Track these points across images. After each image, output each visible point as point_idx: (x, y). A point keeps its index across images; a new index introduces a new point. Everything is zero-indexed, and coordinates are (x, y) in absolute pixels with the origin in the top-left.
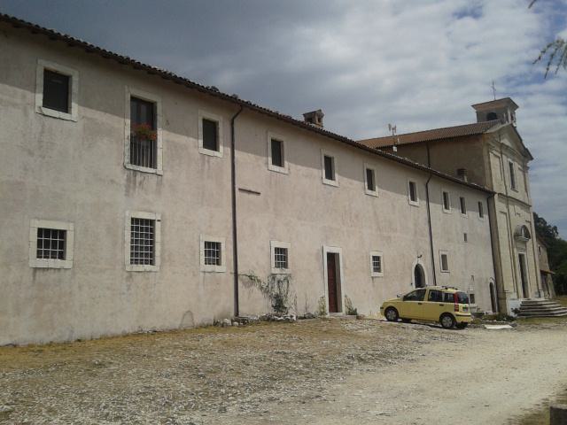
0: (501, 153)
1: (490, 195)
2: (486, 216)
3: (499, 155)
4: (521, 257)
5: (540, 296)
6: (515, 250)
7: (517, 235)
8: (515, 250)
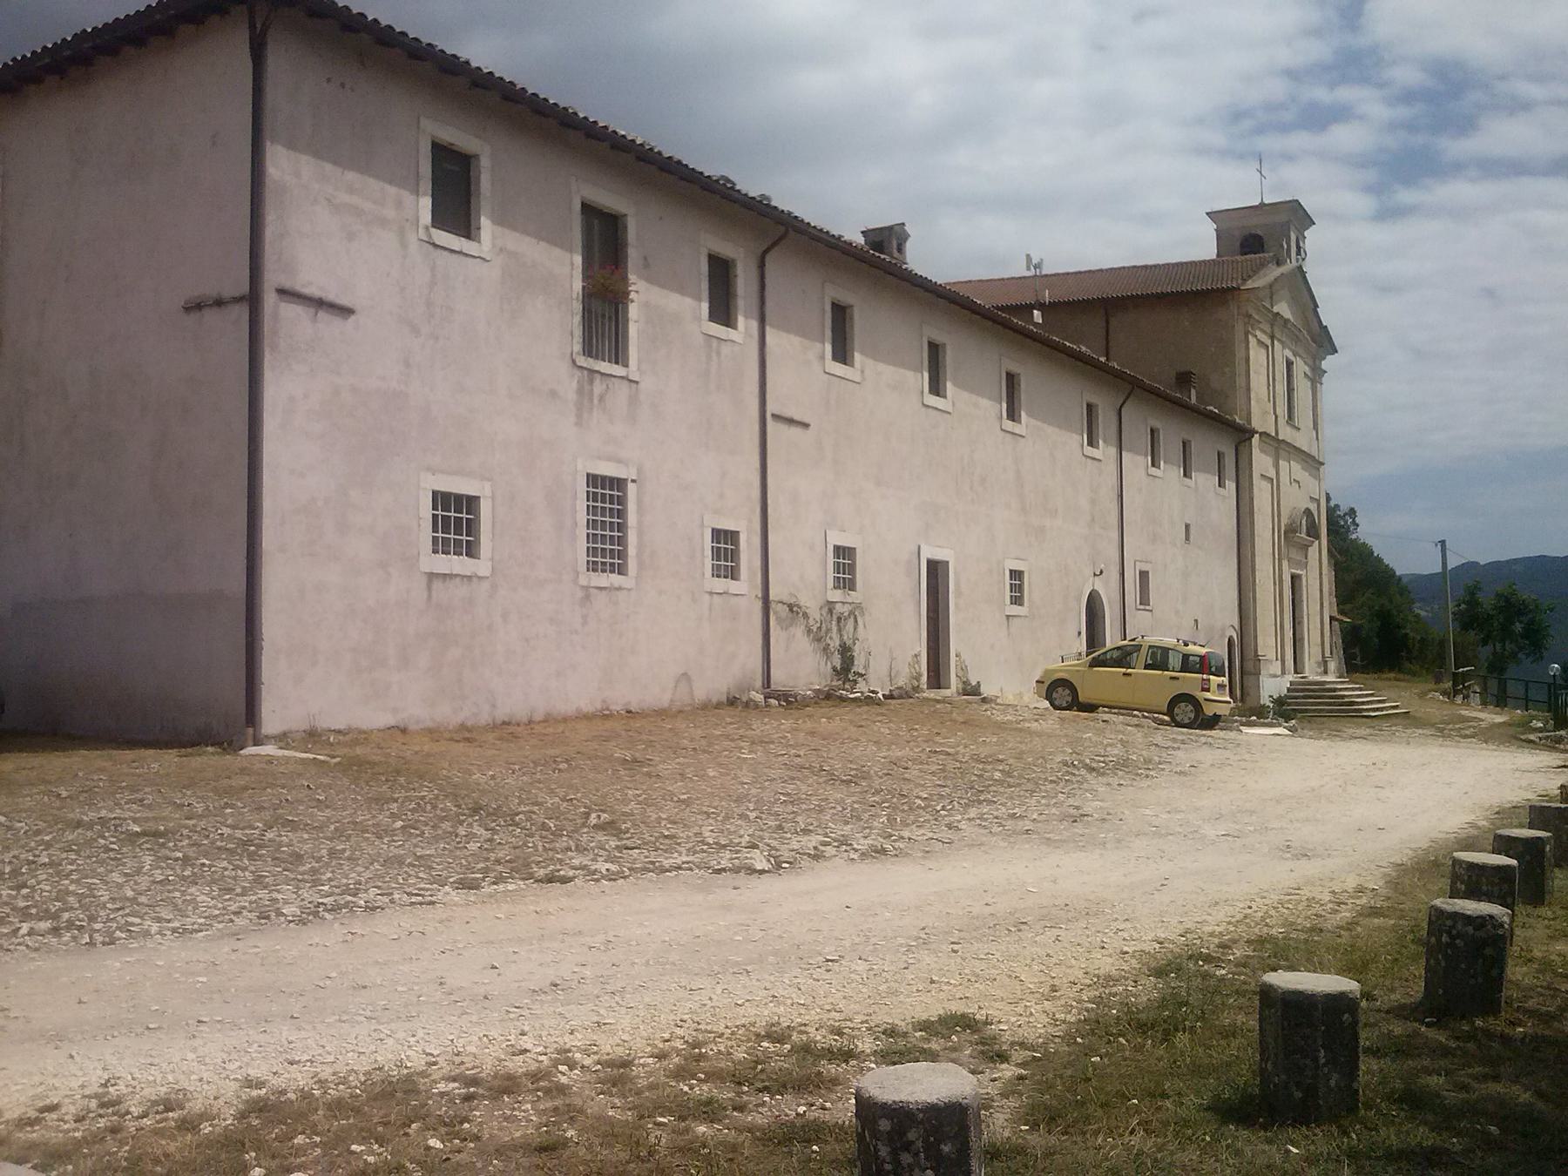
0: (1272, 338)
1: (1242, 435)
2: (1231, 485)
3: (1268, 342)
4: (1295, 579)
5: (1326, 672)
6: (1285, 563)
7: (1291, 530)
8: (1285, 563)
